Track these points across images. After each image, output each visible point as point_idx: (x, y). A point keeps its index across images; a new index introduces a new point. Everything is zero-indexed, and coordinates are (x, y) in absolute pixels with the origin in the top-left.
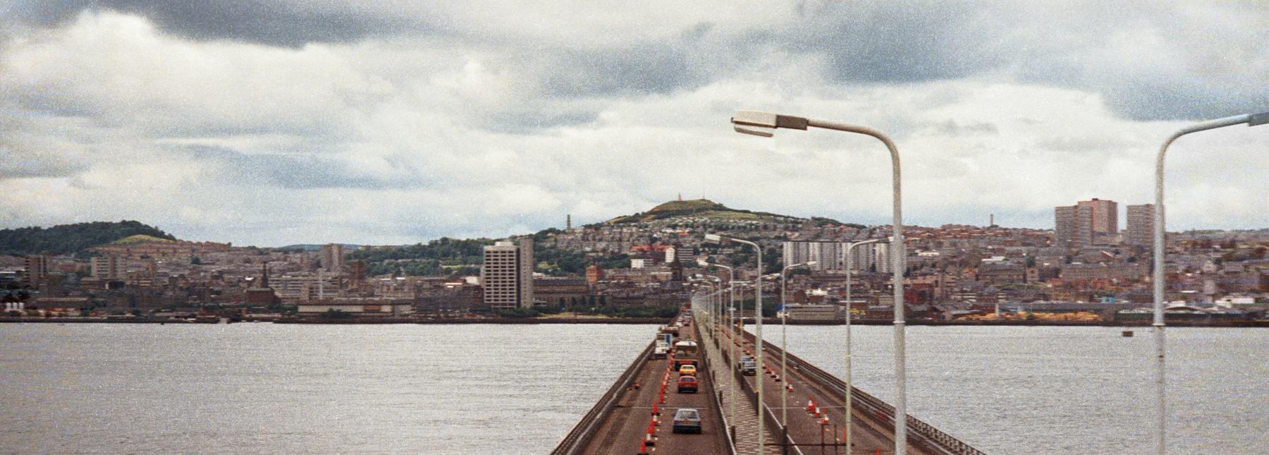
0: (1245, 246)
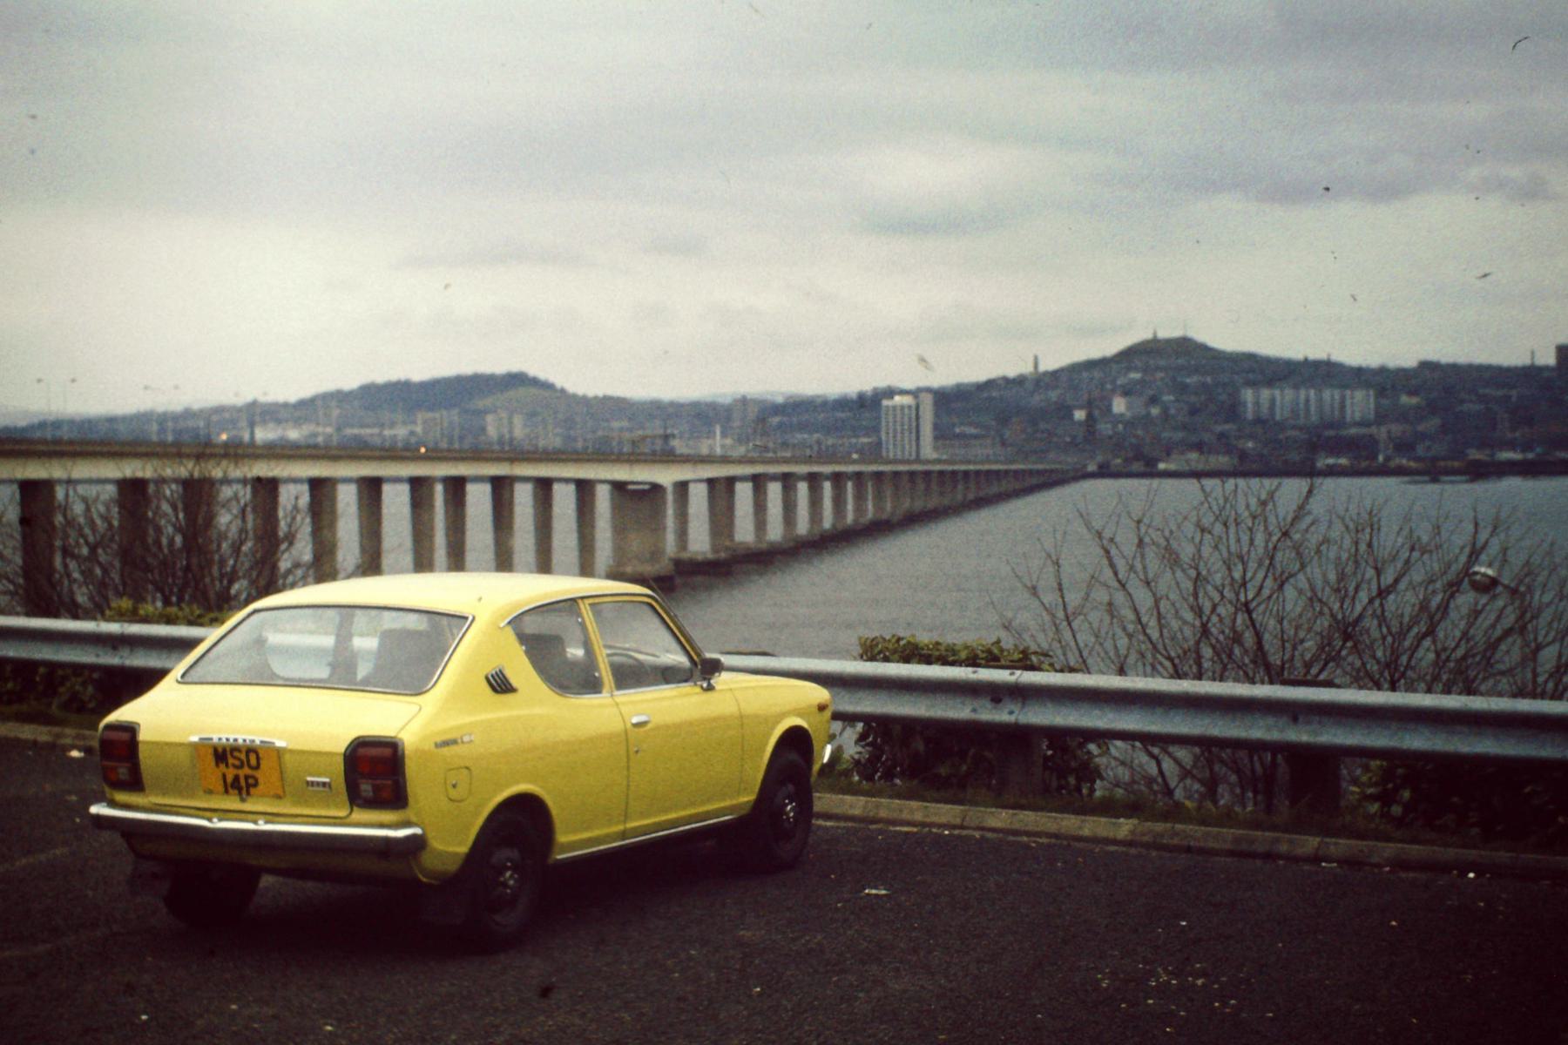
0: (1414, 400)
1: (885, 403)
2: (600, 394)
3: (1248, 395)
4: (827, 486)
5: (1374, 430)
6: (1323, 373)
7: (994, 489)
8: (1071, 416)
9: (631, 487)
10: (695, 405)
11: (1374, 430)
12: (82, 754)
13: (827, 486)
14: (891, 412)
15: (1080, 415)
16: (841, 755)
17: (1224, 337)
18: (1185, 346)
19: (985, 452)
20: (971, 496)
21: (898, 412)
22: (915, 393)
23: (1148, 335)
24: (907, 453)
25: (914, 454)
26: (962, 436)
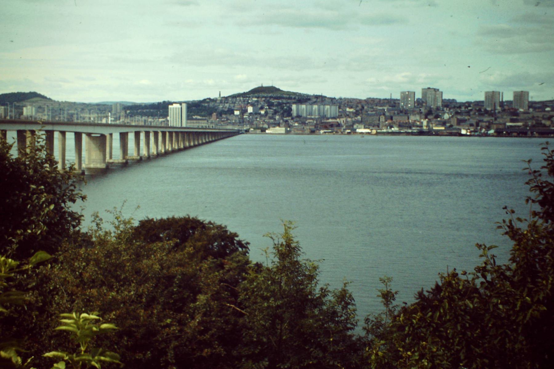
1: (170, 106)
2: (64, 101)
3: (294, 107)
4: (174, 134)
5: (338, 120)
6: (320, 99)
7: (224, 136)
8: (233, 113)
9: (93, 135)
10: (98, 105)
11: (338, 120)
12: (537, 280)
13: (174, 134)
14: (172, 110)
15: (237, 113)
16: (248, 259)
17: (285, 87)
18: (272, 89)
19: (205, 125)
20: (192, 144)
21: (172, 110)
22: (180, 103)
23: (260, 85)
24: (175, 123)
25: (180, 125)
26: (196, 119)
